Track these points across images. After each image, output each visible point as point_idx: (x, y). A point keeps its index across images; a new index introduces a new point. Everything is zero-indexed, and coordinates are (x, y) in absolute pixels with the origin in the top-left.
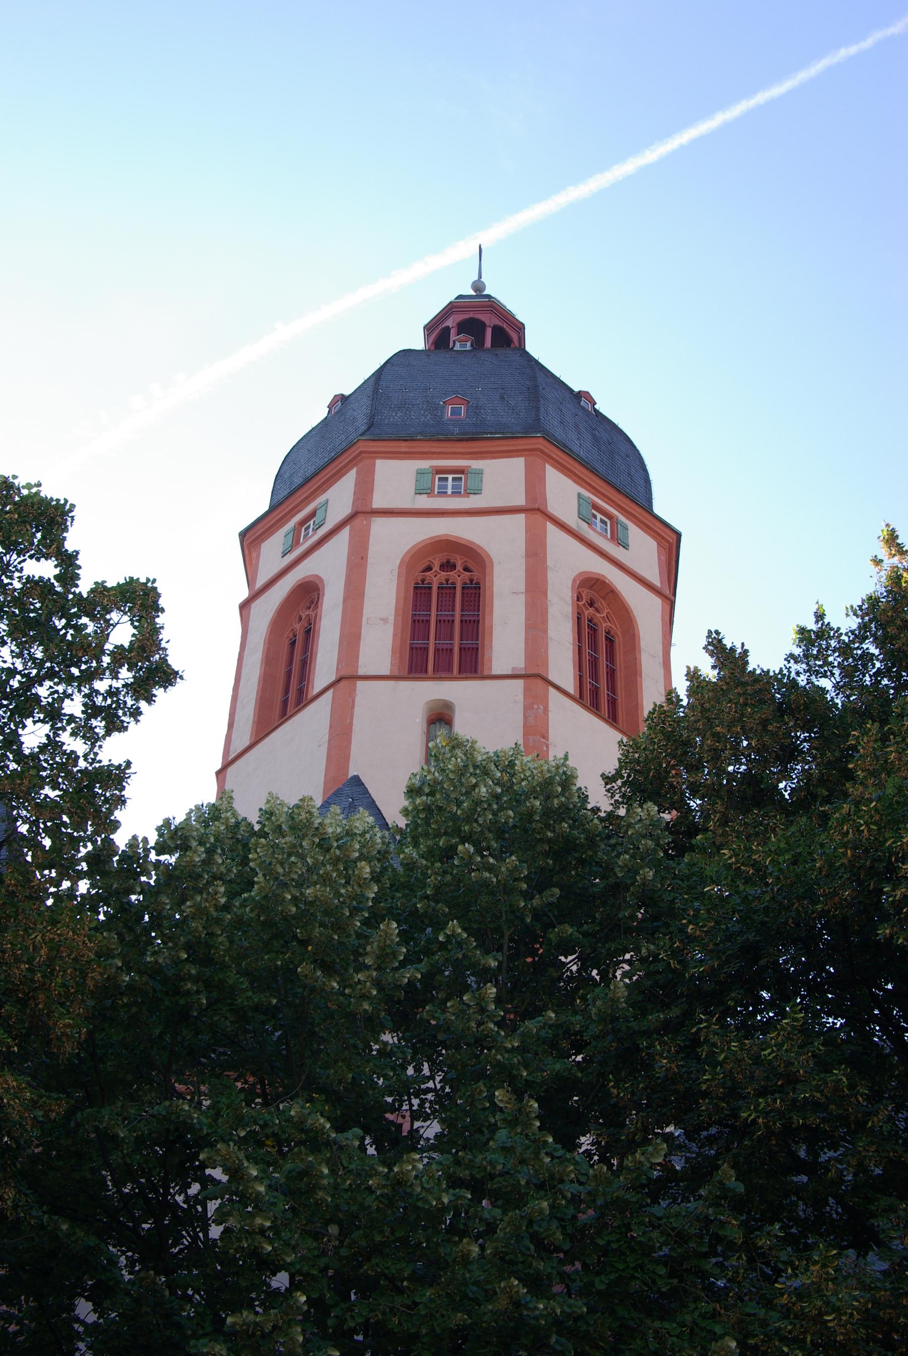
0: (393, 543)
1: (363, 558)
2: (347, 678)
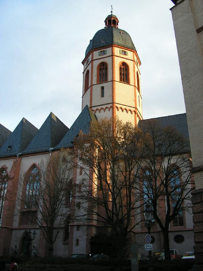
0: (96, 63)
1: (93, 67)
2: (92, 85)
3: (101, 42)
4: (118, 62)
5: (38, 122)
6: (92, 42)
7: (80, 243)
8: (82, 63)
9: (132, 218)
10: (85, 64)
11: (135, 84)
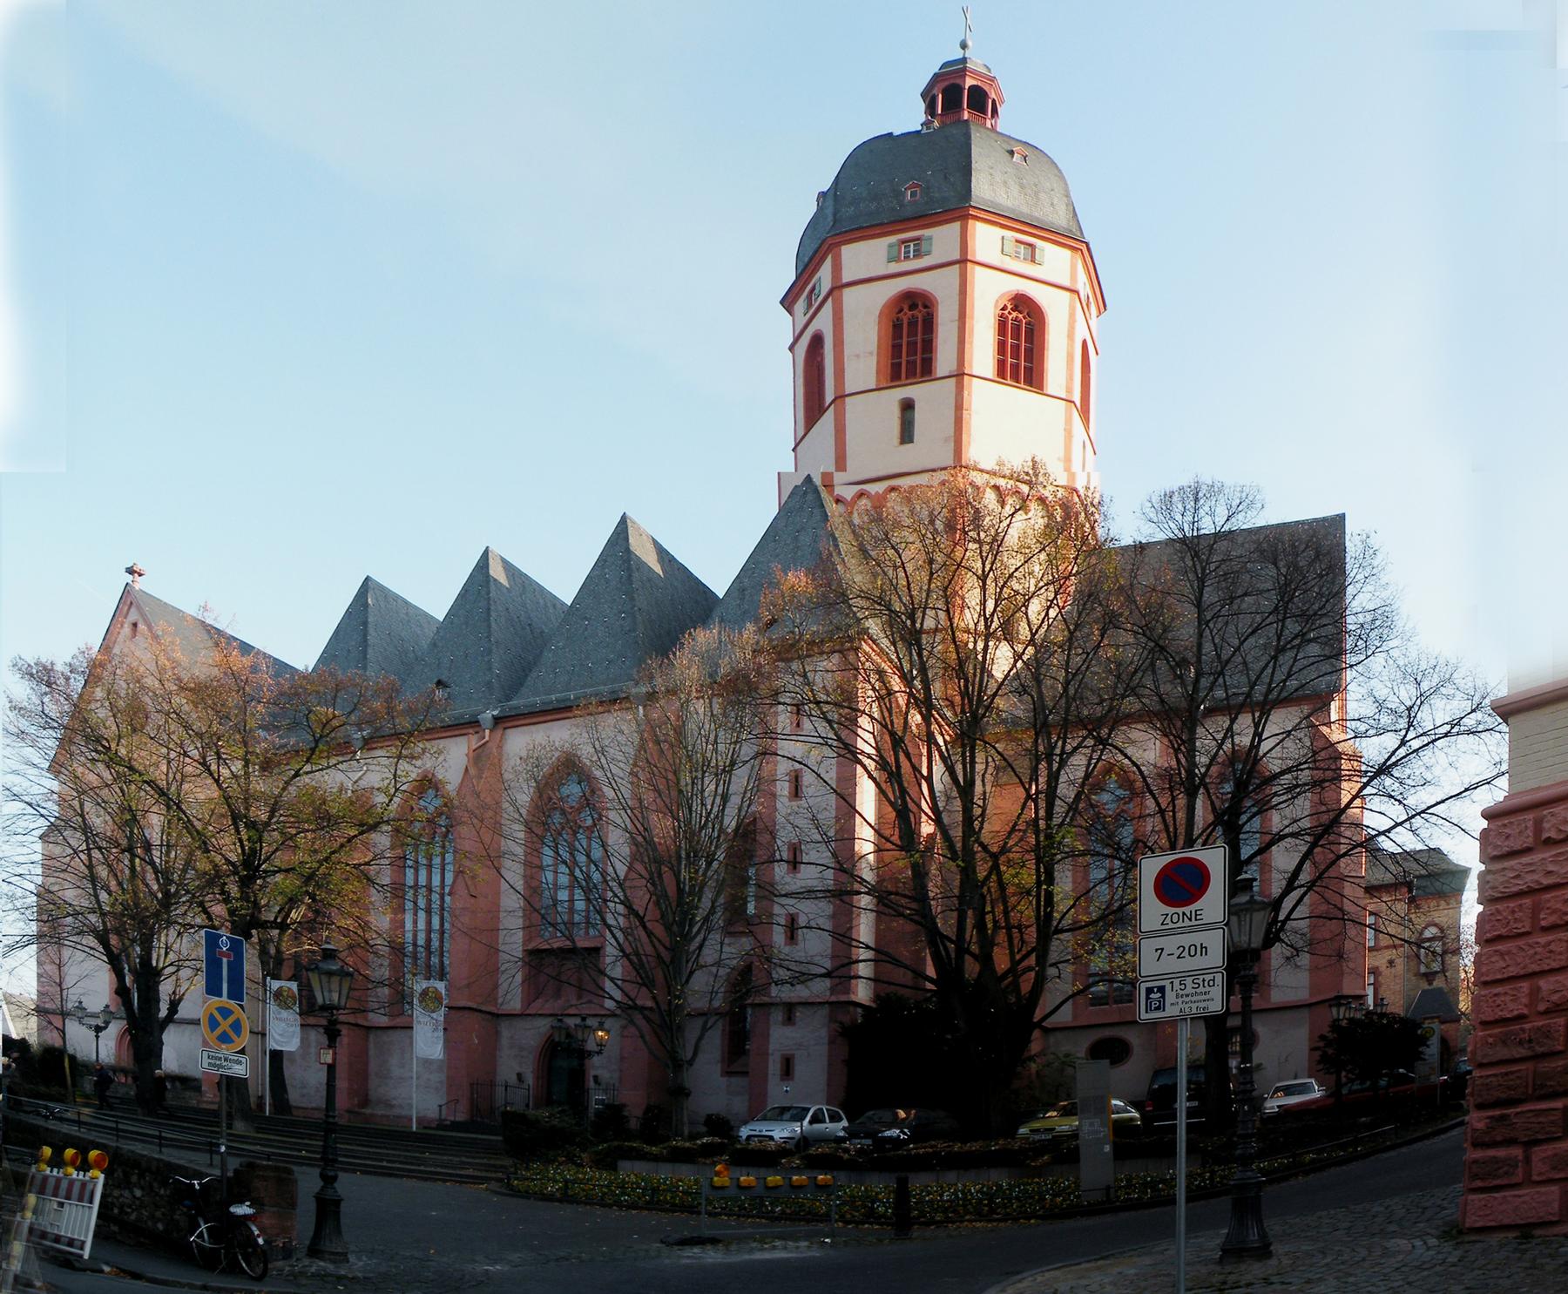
1: (841, 318)
3: (903, 195)
4: (988, 295)
5: (434, 593)
6: (830, 202)
7: (799, 1069)
8: (782, 302)
9: (1052, 971)
10: (800, 305)
11: (1069, 390)
